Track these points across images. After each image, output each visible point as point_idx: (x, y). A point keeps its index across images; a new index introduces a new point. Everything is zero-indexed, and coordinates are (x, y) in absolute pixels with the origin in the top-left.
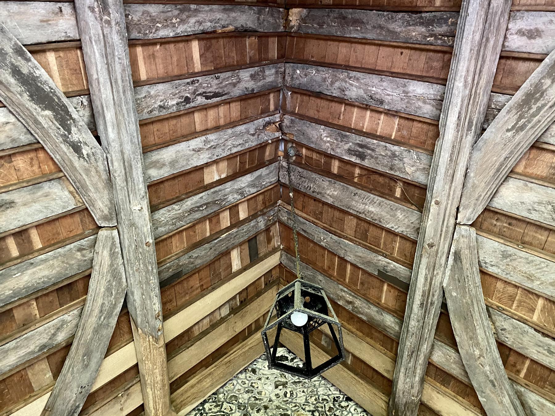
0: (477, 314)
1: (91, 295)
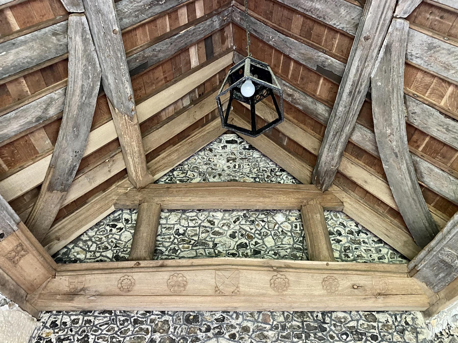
0: (395, 100)
1: (71, 77)
